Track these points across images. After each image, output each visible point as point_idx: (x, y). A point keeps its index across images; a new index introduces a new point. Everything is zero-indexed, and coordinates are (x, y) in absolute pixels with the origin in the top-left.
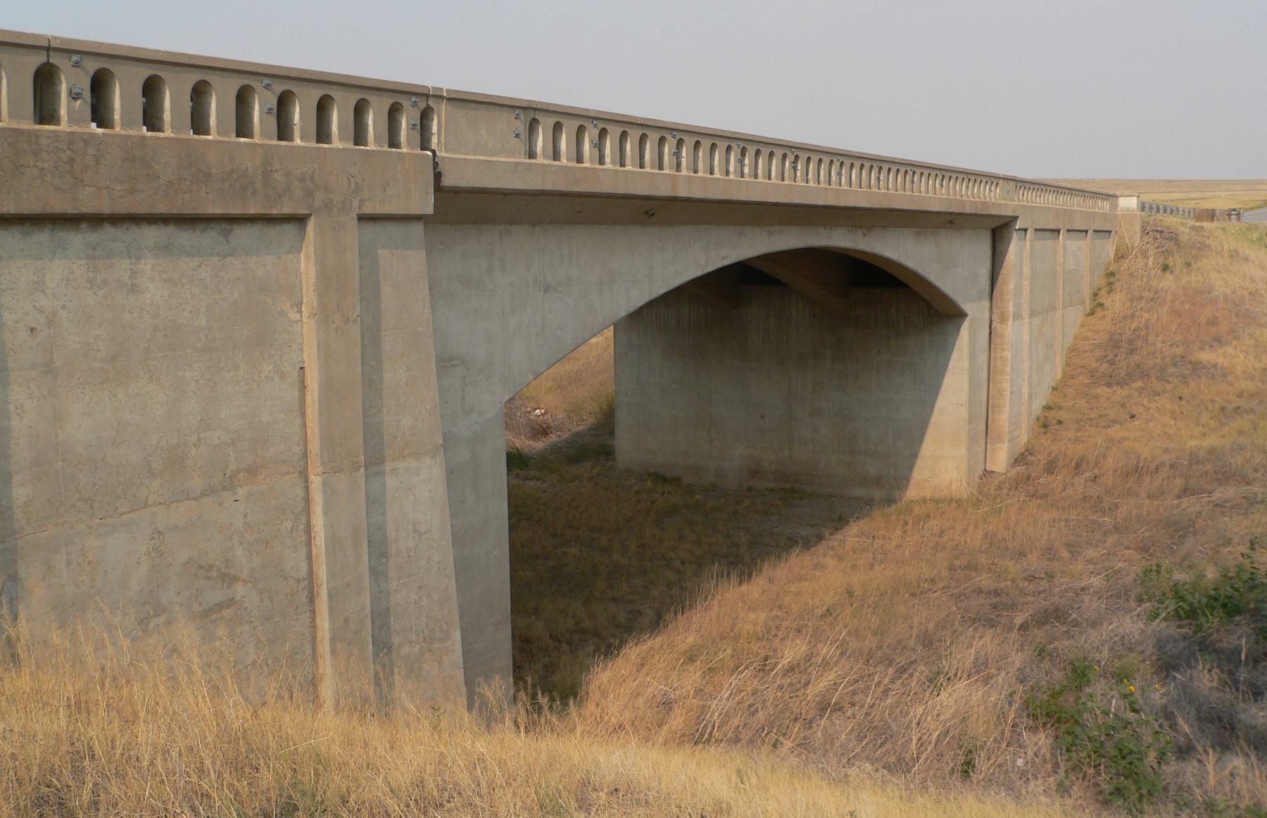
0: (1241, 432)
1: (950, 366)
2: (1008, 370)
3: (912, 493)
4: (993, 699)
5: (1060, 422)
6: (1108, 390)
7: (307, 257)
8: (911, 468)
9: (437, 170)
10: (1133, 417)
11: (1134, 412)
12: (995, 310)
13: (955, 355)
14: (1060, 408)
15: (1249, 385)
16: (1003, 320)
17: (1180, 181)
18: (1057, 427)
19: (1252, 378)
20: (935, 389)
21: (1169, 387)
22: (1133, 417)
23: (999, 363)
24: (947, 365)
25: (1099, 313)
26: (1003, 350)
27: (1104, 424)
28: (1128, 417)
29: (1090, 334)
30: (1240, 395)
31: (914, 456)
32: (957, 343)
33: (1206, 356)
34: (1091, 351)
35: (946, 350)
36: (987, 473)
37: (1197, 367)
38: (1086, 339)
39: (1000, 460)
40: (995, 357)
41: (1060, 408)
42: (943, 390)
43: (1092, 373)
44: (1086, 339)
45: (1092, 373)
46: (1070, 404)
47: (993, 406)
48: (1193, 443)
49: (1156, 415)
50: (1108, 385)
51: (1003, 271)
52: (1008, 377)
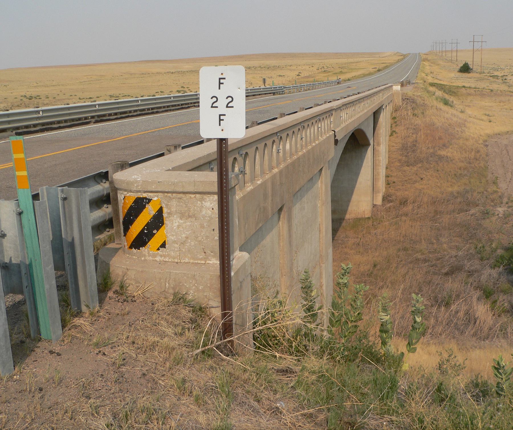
0: (465, 184)
1: (364, 165)
2: (381, 164)
3: (347, 216)
4: (173, 254)
5: (394, 182)
6: (408, 168)
7: (322, 183)
8: (348, 206)
9: (336, 138)
10: (422, 179)
11: (422, 177)
12: (375, 141)
13: (365, 161)
14: (391, 176)
15: (462, 165)
16: (379, 144)
17: (341, 53)
18: (394, 184)
19: (463, 162)
20: (357, 174)
21: (432, 166)
22: (422, 179)
23: (377, 162)
24: (362, 165)
25: (395, 135)
26: (379, 156)
27: (412, 182)
28: (419, 179)
29: (394, 144)
30: (460, 169)
31: (349, 201)
32: (366, 156)
33: (443, 153)
34: (397, 151)
35: (362, 159)
36: (374, 206)
37: (441, 158)
38: (393, 146)
39: (379, 201)
40: (376, 159)
41: (391, 176)
42: (361, 174)
43: (400, 161)
44: (393, 146)
45: (400, 161)
46: (396, 174)
47: (375, 179)
48: (450, 189)
49: (431, 178)
50: (408, 166)
51: (378, 125)
52: (381, 167)
